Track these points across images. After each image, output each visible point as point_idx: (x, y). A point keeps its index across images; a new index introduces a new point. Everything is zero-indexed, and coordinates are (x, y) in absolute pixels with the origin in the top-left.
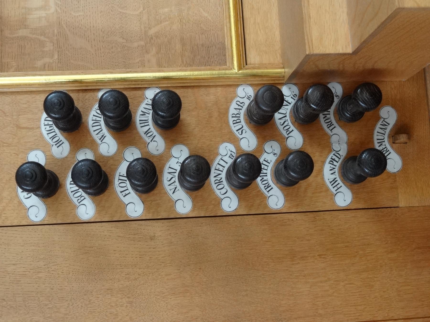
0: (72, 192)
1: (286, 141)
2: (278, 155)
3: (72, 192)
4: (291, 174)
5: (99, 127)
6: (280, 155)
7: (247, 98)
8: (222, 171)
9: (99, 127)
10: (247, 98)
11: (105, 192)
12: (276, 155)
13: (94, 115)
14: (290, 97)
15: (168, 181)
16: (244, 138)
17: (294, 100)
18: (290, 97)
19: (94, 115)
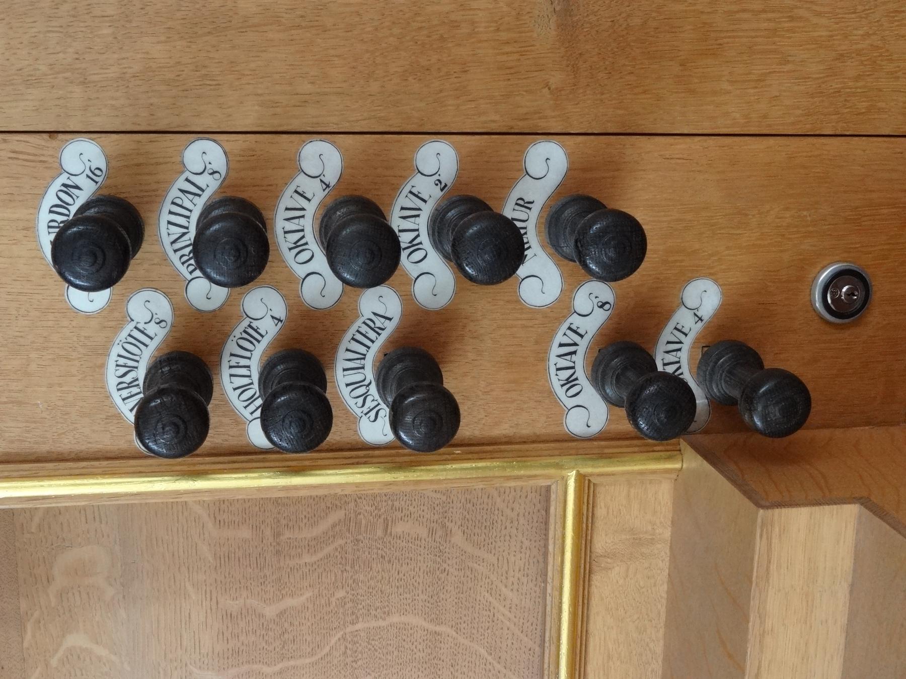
0: (347, 385)
1: (302, 286)
2: (169, 324)
3: (347, 385)
4: (282, 395)
5: (362, 350)
6: (172, 326)
7: (88, 176)
8: (262, 336)
9: (362, 350)
10: (88, 176)
11: (140, 215)
12: (163, 324)
13: (119, 356)
14: (84, 175)
15: (373, 422)
16: (300, 264)
17: (97, 183)
18: (84, 175)
19: (119, 356)
